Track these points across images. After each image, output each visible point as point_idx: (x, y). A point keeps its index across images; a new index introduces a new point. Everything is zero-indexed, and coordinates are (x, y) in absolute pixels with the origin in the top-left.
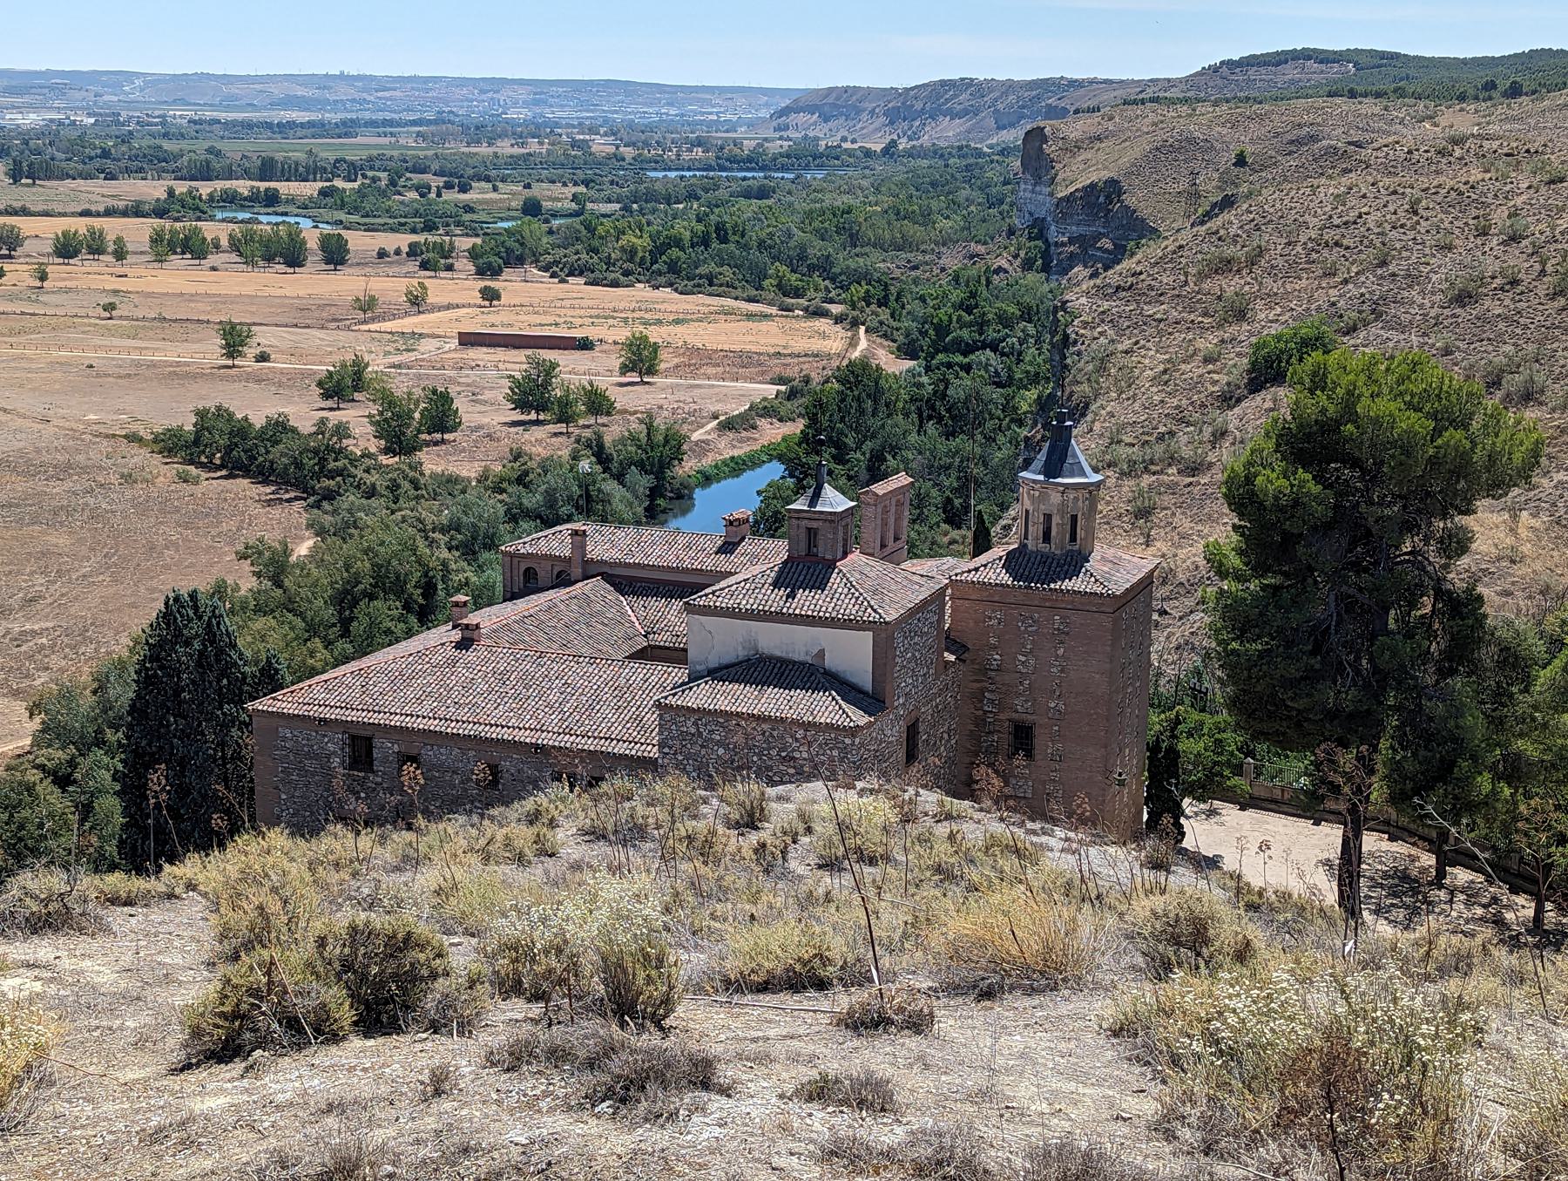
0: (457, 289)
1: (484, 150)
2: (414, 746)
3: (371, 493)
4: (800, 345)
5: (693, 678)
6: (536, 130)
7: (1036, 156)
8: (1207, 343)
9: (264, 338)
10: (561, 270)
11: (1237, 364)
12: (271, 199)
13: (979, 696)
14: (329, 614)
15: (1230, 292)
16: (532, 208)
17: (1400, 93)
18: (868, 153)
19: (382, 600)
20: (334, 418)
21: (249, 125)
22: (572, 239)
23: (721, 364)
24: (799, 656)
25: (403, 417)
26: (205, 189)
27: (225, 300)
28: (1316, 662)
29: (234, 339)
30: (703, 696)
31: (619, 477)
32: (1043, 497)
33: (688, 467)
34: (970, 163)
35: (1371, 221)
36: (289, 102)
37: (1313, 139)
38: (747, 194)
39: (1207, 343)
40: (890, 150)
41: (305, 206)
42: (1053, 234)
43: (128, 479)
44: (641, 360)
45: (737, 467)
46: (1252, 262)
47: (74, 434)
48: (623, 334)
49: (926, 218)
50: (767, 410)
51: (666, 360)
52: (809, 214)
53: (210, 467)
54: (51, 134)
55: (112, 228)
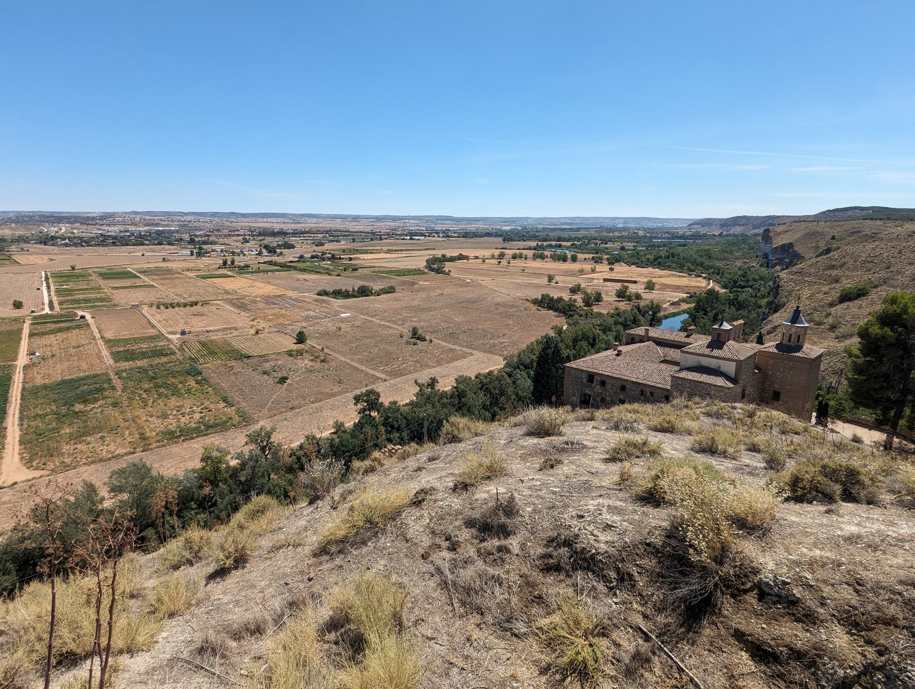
0: (603, 268)
1: (611, 234)
2: (604, 381)
3: (581, 316)
4: (693, 284)
5: (681, 370)
6: (624, 229)
7: (767, 236)
8: (826, 288)
9: (557, 278)
10: (629, 264)
11: (835, 295)
12: (560, 246)
13: (764, 382)
14: (571, 343)
15: (833, 275)
16: (623, 248)
17: (889, 219)
18: (714, 235)
19: (591, 343)
20: (574, 297)
21: (555, 229)
22: (632, 256)
23: (672, 288)
24: (713, 367)
25: (589, 298)
26: (545, 244)
27: (549, 269)
28: (885, 384)
29: (550, 278)
30: (684, 374)
31: (643, 316)
32: (790, 329)
33: (662, 314)
34: (744, 238)
35: (884, 256)
36: (565, 224)
37: (858, 232)
38: (680, 246)
39: (826, 288)
40: (720, 235)
41: (567, 248)
42: (770, 257)
43: (526, 309)
44: (650, 286)
45: (674, 315)
46: (841, 266)
47: (514, 298)
48: (646, 280)
49: (731, 252)
50: (683, 300)
51: (657, 287)
52: (698, 251)
53: (544, 307)
54: (512, 231)
55: (525, 252)
